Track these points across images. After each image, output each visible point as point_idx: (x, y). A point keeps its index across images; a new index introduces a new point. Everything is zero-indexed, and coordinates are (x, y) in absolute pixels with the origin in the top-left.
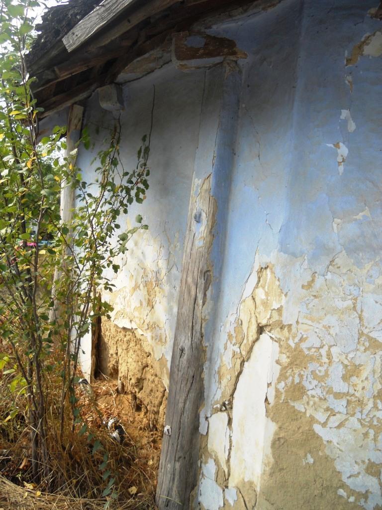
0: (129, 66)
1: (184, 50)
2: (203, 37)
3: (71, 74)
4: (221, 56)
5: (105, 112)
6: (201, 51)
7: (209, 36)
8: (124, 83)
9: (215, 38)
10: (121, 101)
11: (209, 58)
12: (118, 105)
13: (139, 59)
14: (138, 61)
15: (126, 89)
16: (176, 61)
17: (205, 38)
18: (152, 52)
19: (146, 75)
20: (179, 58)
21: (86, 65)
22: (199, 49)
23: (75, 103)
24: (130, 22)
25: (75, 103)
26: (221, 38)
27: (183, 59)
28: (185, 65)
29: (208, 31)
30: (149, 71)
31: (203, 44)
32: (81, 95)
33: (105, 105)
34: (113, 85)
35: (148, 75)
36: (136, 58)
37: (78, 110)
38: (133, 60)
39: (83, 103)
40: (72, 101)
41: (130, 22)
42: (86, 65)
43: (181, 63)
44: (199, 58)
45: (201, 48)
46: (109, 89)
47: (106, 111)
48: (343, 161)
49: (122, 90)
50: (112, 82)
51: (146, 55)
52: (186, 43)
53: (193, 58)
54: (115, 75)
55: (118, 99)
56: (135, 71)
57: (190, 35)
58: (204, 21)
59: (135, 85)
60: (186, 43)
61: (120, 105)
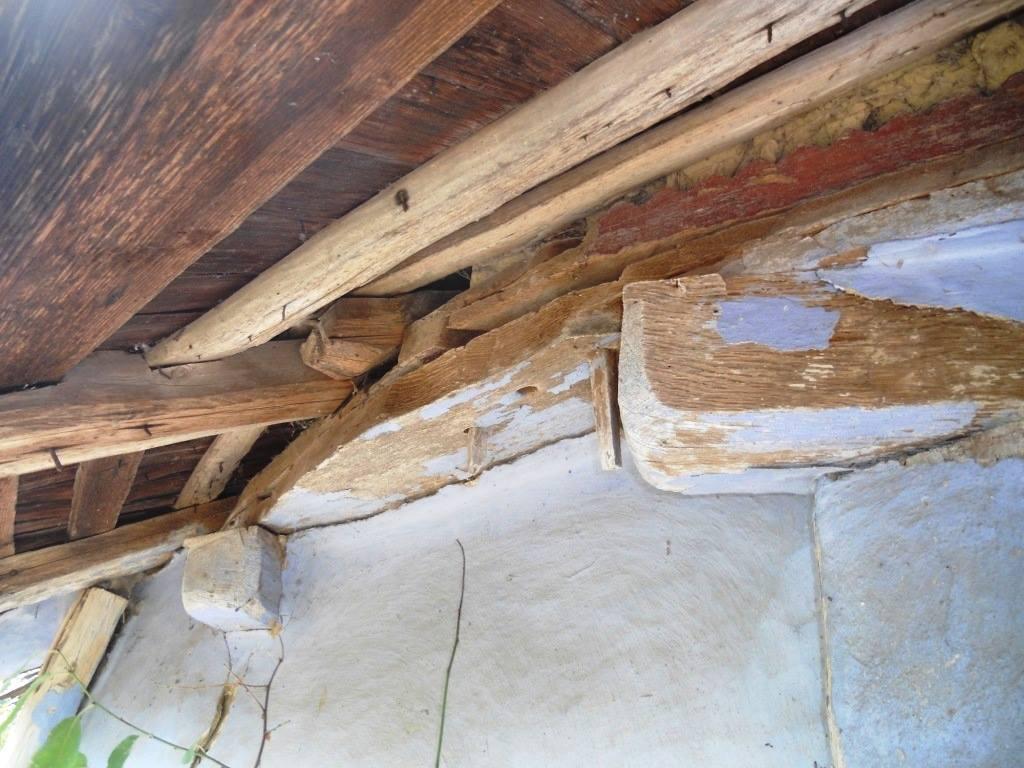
0: (336, 456)
1: (709, 357)
2: (813, 305)
3: (53, 450)
4: (959, 397)
5: (198, 632)
6: (818, 371)
7: (846, 301)
8: (298, 530)
9: (889, 309)
10: (272, 595)
11: (879, 405)
12: (258, 609)
13: (393, 425)
14: (385, 436)
15: (293, 545)
16: (661, 410)
17: (827, 307)
18: (465, 394)
19: (397, 505)
20: (674, 395)
21: (139, 420)
22: (801, 358)
23: (98, 584)
24: (406, 208)
25: (98, 584)
26: (935, 313)
27: (708, 404)
28: (717, 436)
29: (842, 280)
30: (417, 489)
31: (829, 333)
32: (127, 558)
33: (200, 606)
34: (255, 529)
35: (405, 508)
36: (381, 421)
37: (106, 608)
38: (364, 430)
39: (130, 590)
40: (90, 574)
41: (406, 208)
42: (139, 420)
43: (690, 425)
44: (805, 403)
45: (811, 352)
46: (235, 545)
47: (205, 626)
48: (254, 523)
49: (283, 554)
50: (251, 522)
51: (430, 412)
52: (712, 325)
53: (772, 403)
54: (266, 500)
55: (260, 588)
56: (358, 483)
57: (733, 294)
58: (814, 233)
59: (339, 540)
60: (712, 325)
61: (263, 610)
